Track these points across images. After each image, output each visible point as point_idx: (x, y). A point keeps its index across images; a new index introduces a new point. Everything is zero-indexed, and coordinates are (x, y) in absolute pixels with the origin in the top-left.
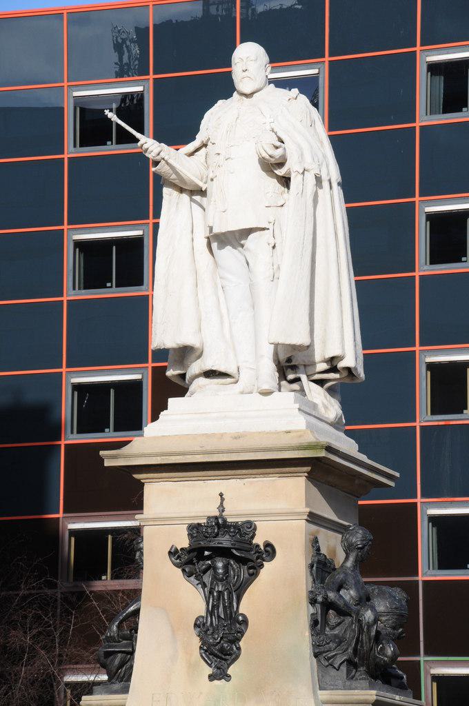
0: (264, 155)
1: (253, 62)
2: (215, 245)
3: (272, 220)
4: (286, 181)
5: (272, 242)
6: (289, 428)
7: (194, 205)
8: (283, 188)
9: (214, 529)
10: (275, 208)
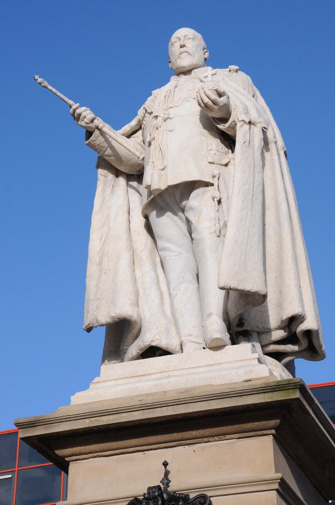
0: (206, 100)
1: (191, 40)
2: (153, 215)
3: (216, 172)
4: (229, 141)
5: (217, 195)
6: (248, 378)
7: (131, 191)
8: (226, 149)
9: (158, 501)
10: (219, 166)
